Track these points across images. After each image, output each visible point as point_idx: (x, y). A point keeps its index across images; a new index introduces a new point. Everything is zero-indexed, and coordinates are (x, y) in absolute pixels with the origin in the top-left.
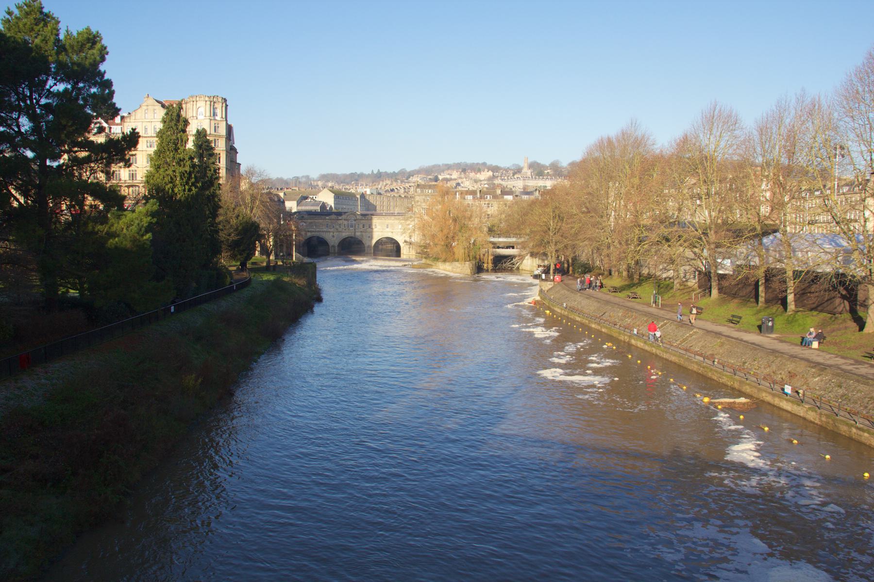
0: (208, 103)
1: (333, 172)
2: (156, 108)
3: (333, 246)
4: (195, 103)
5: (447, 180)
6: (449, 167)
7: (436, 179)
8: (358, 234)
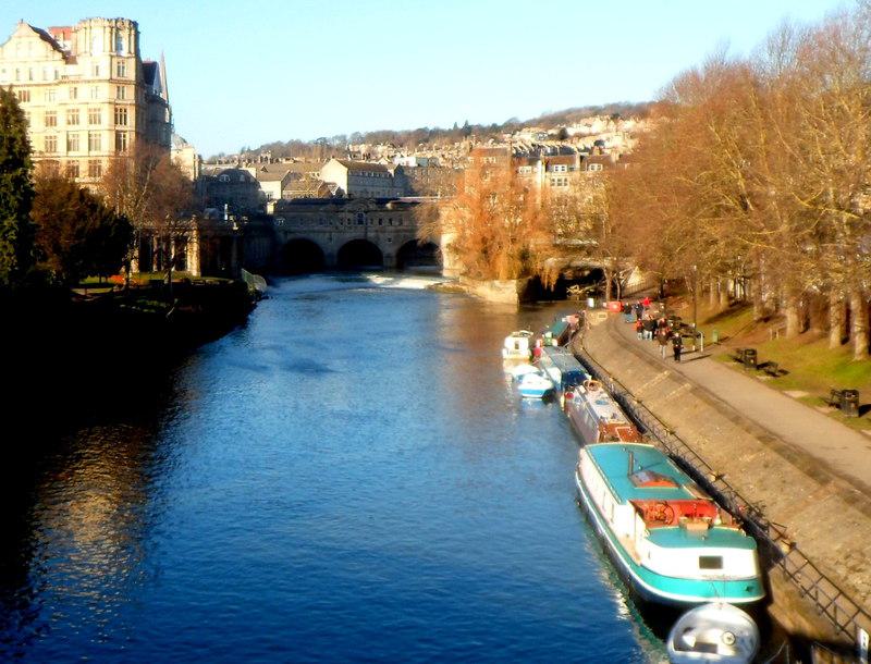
0: (108, 30)
1: (388, 128)
2: (31, 39)
3: (389, 256)
4: (88, 30)
5: (580, 136)
6: (595, 112)
7: (563, 136)
8: (371, 235)
